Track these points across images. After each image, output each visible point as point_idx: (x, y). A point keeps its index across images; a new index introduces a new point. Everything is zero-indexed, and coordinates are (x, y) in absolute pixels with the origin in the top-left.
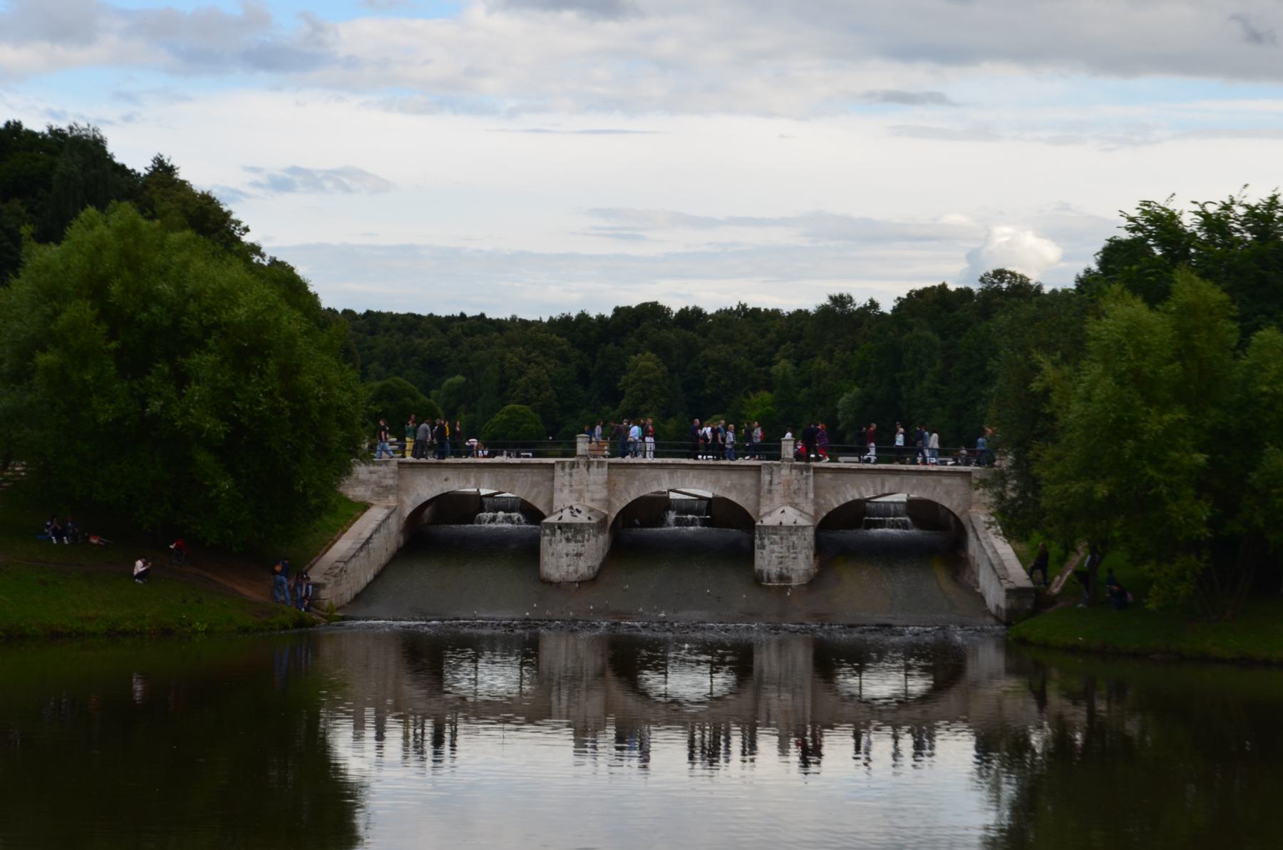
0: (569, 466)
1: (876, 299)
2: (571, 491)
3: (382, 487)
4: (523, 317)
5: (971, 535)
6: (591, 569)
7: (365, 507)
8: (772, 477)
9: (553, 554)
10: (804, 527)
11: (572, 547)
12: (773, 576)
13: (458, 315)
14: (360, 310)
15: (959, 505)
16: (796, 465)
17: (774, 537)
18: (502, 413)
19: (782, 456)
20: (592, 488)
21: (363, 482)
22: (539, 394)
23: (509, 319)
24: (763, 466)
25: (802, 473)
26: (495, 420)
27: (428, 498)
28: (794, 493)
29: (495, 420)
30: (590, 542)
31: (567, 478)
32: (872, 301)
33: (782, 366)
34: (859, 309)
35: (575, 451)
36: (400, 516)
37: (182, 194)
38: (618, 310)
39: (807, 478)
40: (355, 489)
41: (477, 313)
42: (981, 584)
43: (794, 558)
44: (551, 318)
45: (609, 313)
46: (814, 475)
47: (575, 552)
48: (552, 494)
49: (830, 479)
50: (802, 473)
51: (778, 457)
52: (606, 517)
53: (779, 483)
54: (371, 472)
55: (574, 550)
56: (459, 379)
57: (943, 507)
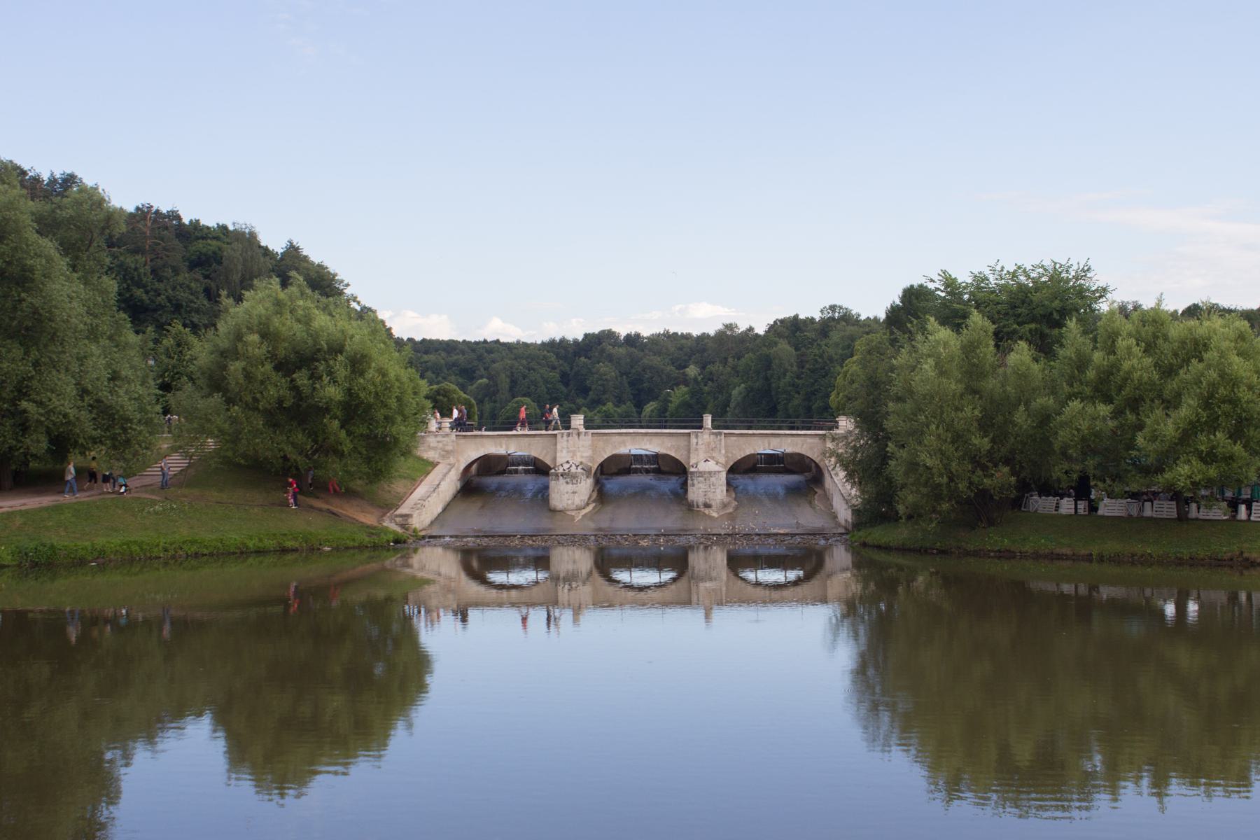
1: (753, 326)
2: (568, 452)
4: (525, 341)
5: (827, 475)
7: (434, 465)
9: (558, 493)
10: (719, 472)
11: (570, 487)
12: (700, 504)
14: (418, 338)
21: (434, 449)
31: (565, 443)
32: (750, 327)
33: (692, 371)
34: (741, 332)
35: (570, 426)
36: (457, 469)
37: (306, 265)
38: (586, 336)
41: (495, 339)
45: (580, 338)
48: (556, 453)
49: (735, 441)
51: (701, 427)
53: (702, 444)
54: (438, 442)
56: (485, 380)
57: (808, 457)
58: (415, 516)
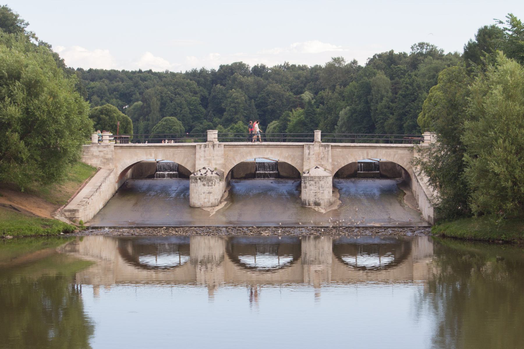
0: (204, 147)
1: (357, 59)
2: (205, 160)
3: (106, 159)
6: (216, 200)
8: (309, 151)
10: (327, 177)
11: (206, 189)
12: (311, 203)
13: (138, 71)
14: (86, 68)
15: (407, 165)
16: (322, 145)
17: (311, 182)
18: (162, 121)
19: (315, 140)
20: (216, 158)
21: (96, 157)
22: (181, 111)
23: (165, 72)
24: (305, 145)
25: (325, 148)
26: (158, 125)
27: (130, 164)
28: (321, 159)
29: (158, 125)
30: (215, 186)
31: (203, 153)
33: (307, 96)
39: (328, 151)
40: (92, 160)
42: (420, 205)
43: (322, 193)
44: (186, 72)
45: (217, 69)
46: (331, 150)
47: (208, 191)
48: (195, 161)
50: (325, 148)
52: (223, 173)
54: (100, 151)
55: (207, 190)
58: (80, 211)
